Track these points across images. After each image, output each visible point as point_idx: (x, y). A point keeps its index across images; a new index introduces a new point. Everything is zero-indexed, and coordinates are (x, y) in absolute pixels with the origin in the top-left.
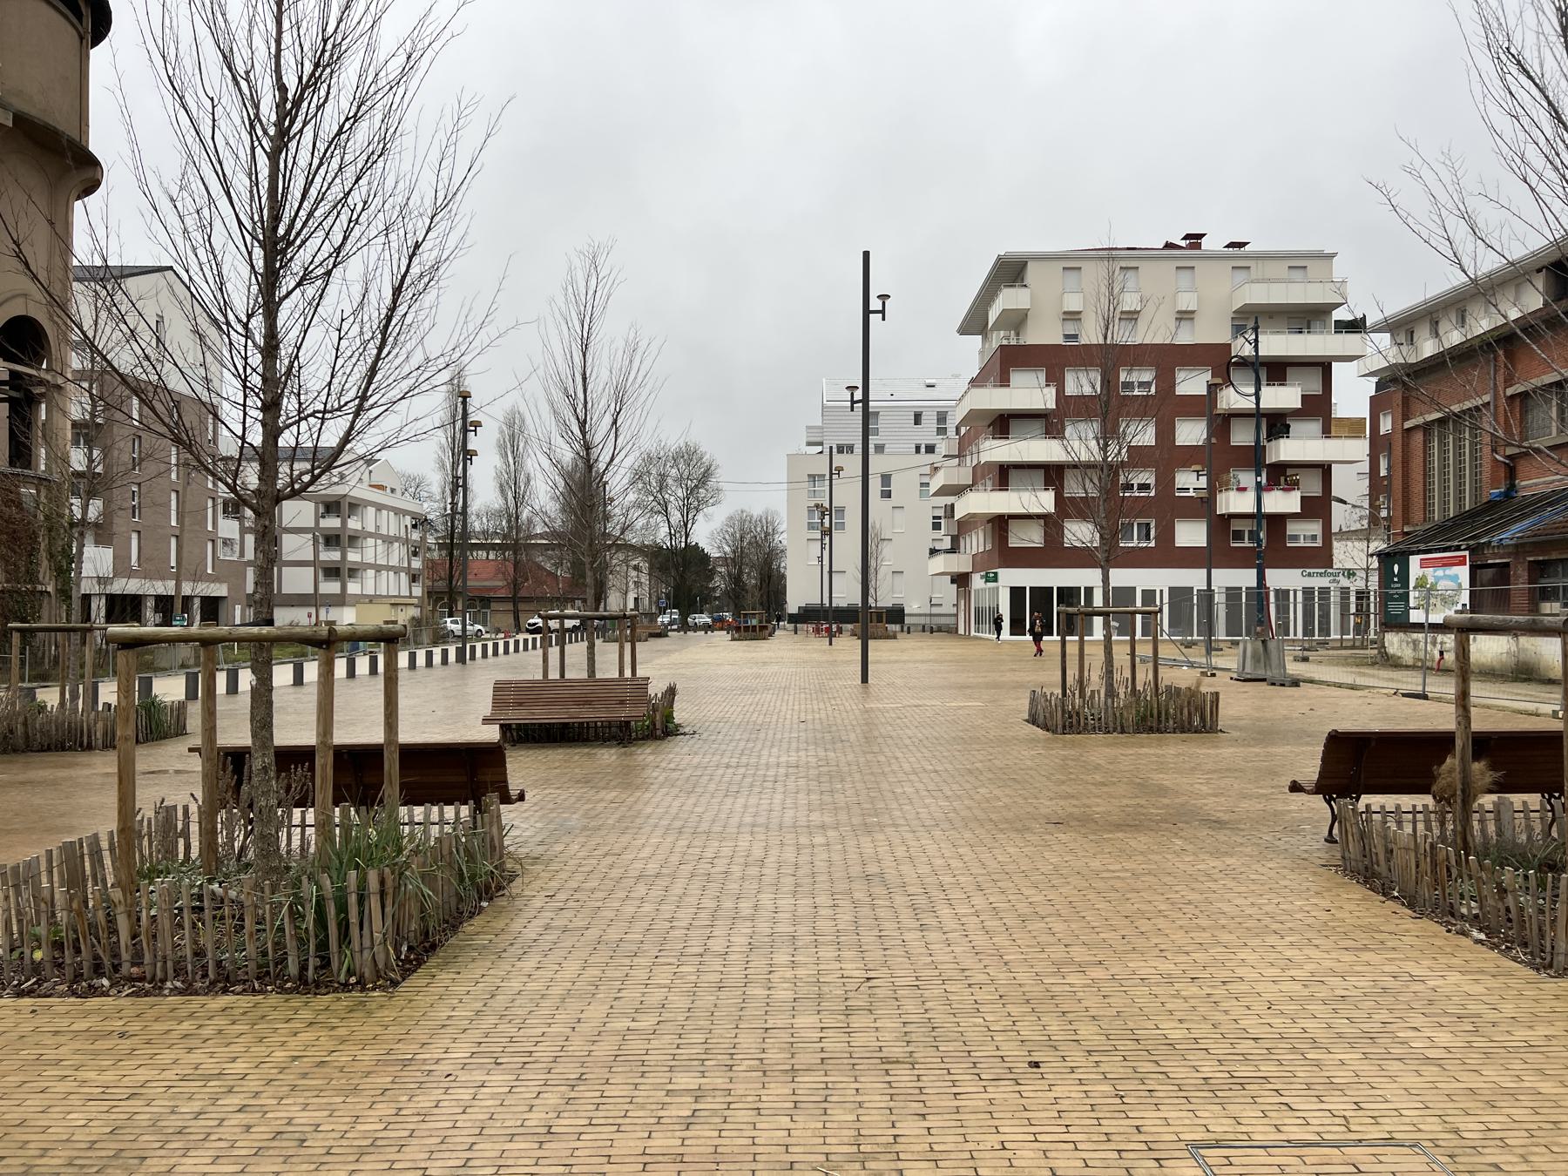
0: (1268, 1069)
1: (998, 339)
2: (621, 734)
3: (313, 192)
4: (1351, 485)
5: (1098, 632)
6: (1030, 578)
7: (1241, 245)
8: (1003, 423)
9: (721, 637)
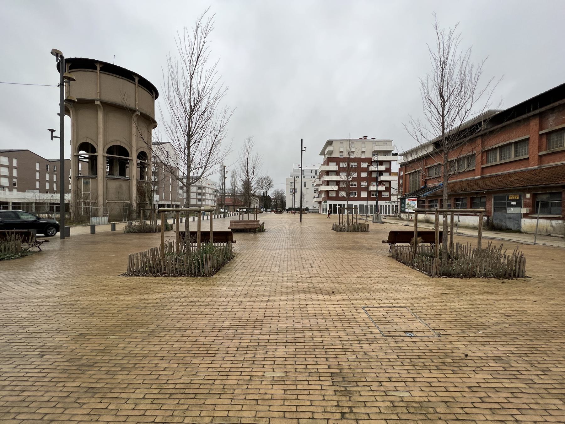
0: (377, 293)
1: (327, 156)
2: (254, 231)
3: (197, 126)
4: (395, 185)
5: (346, 213)
8: (328, 173)
9: (273, 213)
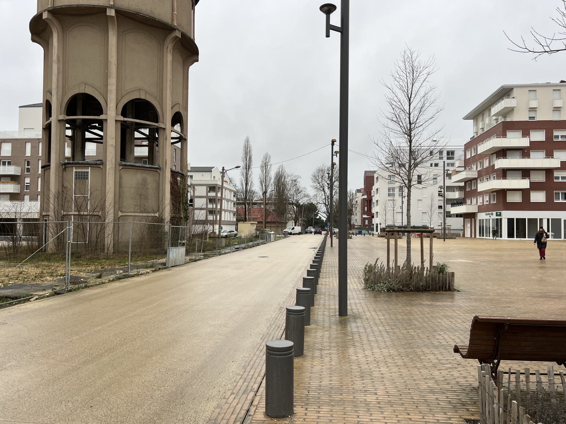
6: (516, 215)
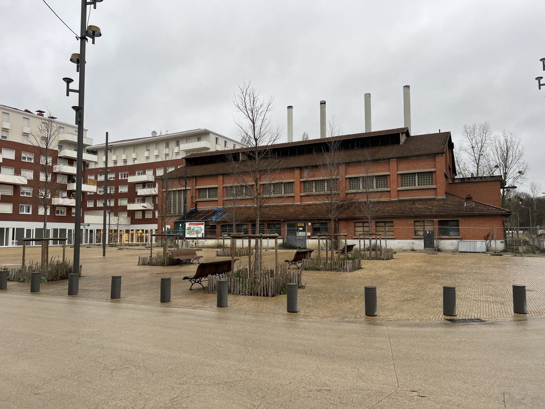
7: (53, 118)
